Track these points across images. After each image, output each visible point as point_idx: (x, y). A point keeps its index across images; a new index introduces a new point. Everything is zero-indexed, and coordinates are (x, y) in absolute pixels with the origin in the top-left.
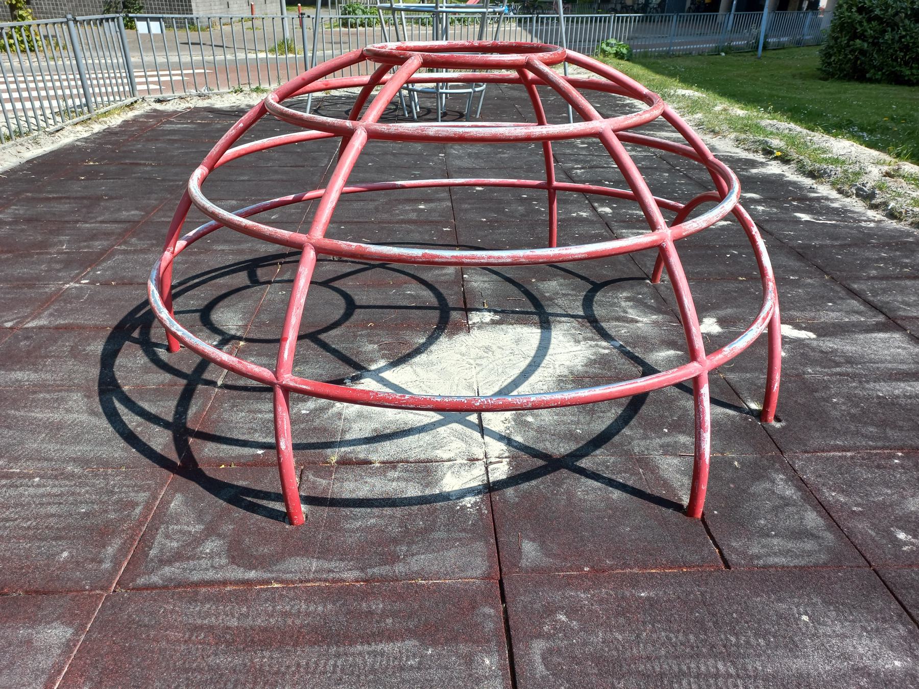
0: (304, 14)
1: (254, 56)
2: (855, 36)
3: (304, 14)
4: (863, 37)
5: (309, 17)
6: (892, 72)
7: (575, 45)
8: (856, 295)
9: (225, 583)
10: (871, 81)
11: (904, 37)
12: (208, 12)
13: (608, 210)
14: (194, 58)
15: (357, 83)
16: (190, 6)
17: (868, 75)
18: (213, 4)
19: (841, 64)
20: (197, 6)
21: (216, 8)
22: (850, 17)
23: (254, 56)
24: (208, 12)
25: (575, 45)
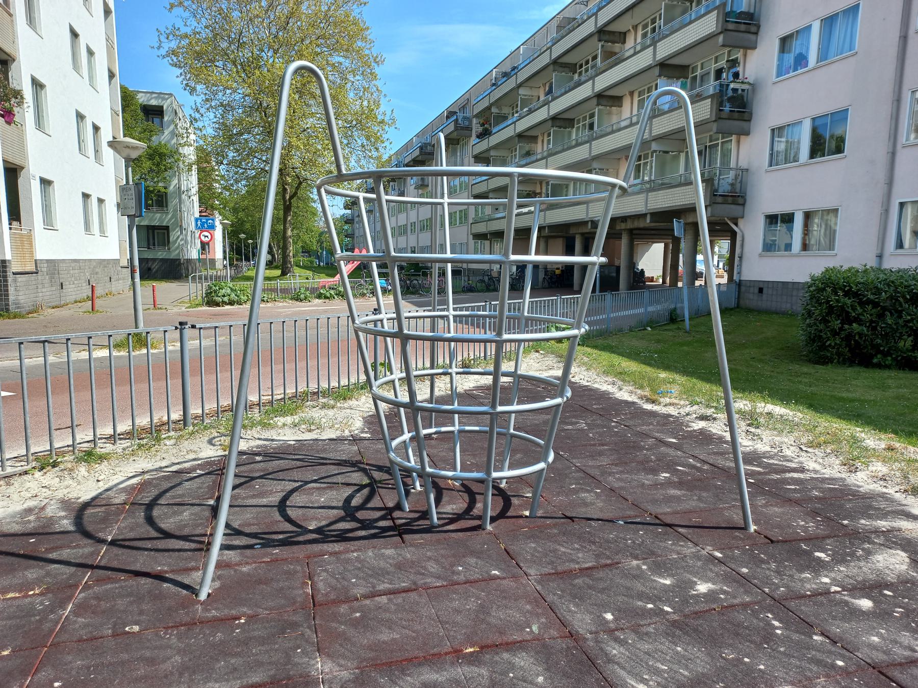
0: (186, 323)
1: (85, 355)
2: (848, 320)
3: (186, 323)
4: (857, 320)
5: (193, 327)
6: (903, 358)
7: (541, 309)
8: (452, 490)
9: (280, 440)
10: (879, 366)
11: (909, 321)
12: (32, 296)
13: (493, 572)
14: (26, 361)
15: (186, 381)
16: (7, 290)
17: (875, 361)
18: (40, 286)
19: (838, 348)
20: (16, 290)
21: (44, 290)
22: (838, 301)
23: (85, 355)
24: (32, 296)
25: (541, 309)
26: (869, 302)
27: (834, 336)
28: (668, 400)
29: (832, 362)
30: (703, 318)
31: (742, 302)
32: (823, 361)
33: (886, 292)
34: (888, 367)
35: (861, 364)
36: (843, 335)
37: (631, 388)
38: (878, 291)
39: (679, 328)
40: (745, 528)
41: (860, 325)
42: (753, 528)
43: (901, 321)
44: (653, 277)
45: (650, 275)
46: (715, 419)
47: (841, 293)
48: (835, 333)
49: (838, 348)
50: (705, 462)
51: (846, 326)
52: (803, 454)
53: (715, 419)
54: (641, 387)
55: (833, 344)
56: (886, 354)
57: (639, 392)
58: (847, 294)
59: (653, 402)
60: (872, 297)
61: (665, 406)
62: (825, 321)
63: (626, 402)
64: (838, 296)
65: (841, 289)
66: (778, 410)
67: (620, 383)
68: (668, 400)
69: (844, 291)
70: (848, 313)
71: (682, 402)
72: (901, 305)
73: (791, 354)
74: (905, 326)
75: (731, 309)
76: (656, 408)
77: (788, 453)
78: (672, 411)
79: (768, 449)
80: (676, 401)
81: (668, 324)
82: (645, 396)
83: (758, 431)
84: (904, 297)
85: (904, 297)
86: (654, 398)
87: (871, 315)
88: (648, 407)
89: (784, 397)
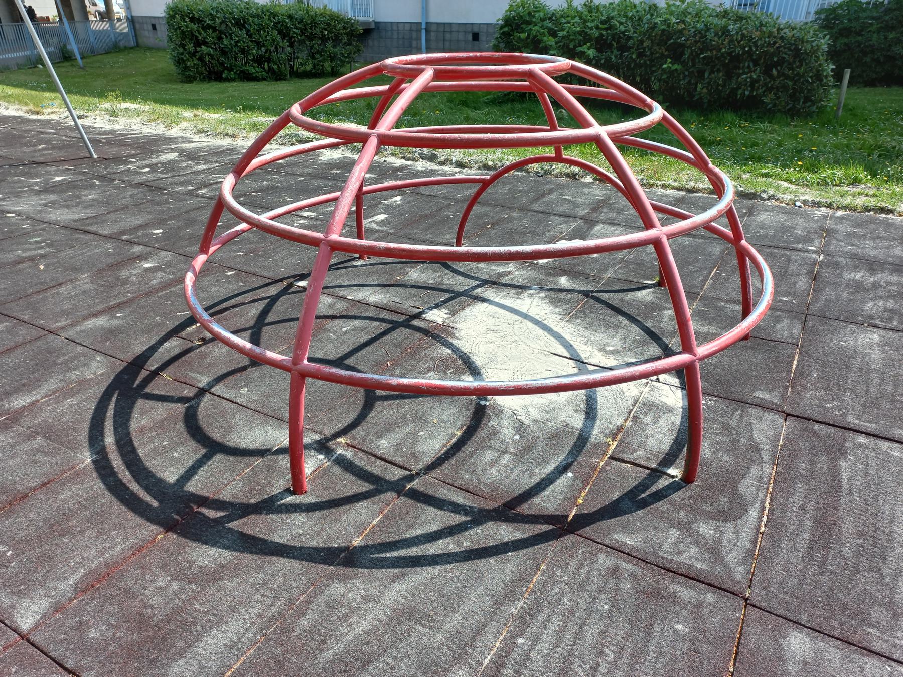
2: (198, 44)
4: (205, 43)
10: (228, 80)
22: (187, 26)
26: (209, 26)
27: (191, 58)
28: (49, 110)
29: (196, 80)
30: (100, 56)
31: (140, 41)
32: (189, 80)
33: (218, 18)
34: (233, 80)
35: (216, 80)
36: (198, 55)
37: (16, 106)
38: (213, 17)
39: (72, 65)
40: (91, 156)
41: (207, 47)
42: (95, 157)
43: (233, 42)
44: (48, 17)
45: (44, 15)
46: (86, 117)
47: (187, 19)
48: (193, 55)
49: (197, 68)
50: (73, 138)
51: (198, 49)
52: (145, 127)
53: (86, 117)
54: (26, 104)
55: (192, 65)
56: (230, 70)
57: (24, 108)
58: (192, 19)
59: (38, 113)
60: (210, 22)
61: (48, 114)
62: (183, 46)
63: (14, 117)
64: (186, 22)
65: (187, 16)
66: (132, 106)
67: (6, 104)
68: (49, 110)
69: (189, 18)
70: (197, 37)
71: (61, 110)
72: (231, 30)
73: (168, 79)
74: (236, 45)
75: (132, 48)
76: (39, 117)
77: (135, 128)
78: (55, 117)
79: (123, 127)
80: (57, 110)
81: (63, 62)
82: (30, 110)
83: (117, 119)
84: (231, 22)
85: (231, 22)
86: (38, 110)
87: (213, 38)
88: (34, 117)
89: (145, 99)
